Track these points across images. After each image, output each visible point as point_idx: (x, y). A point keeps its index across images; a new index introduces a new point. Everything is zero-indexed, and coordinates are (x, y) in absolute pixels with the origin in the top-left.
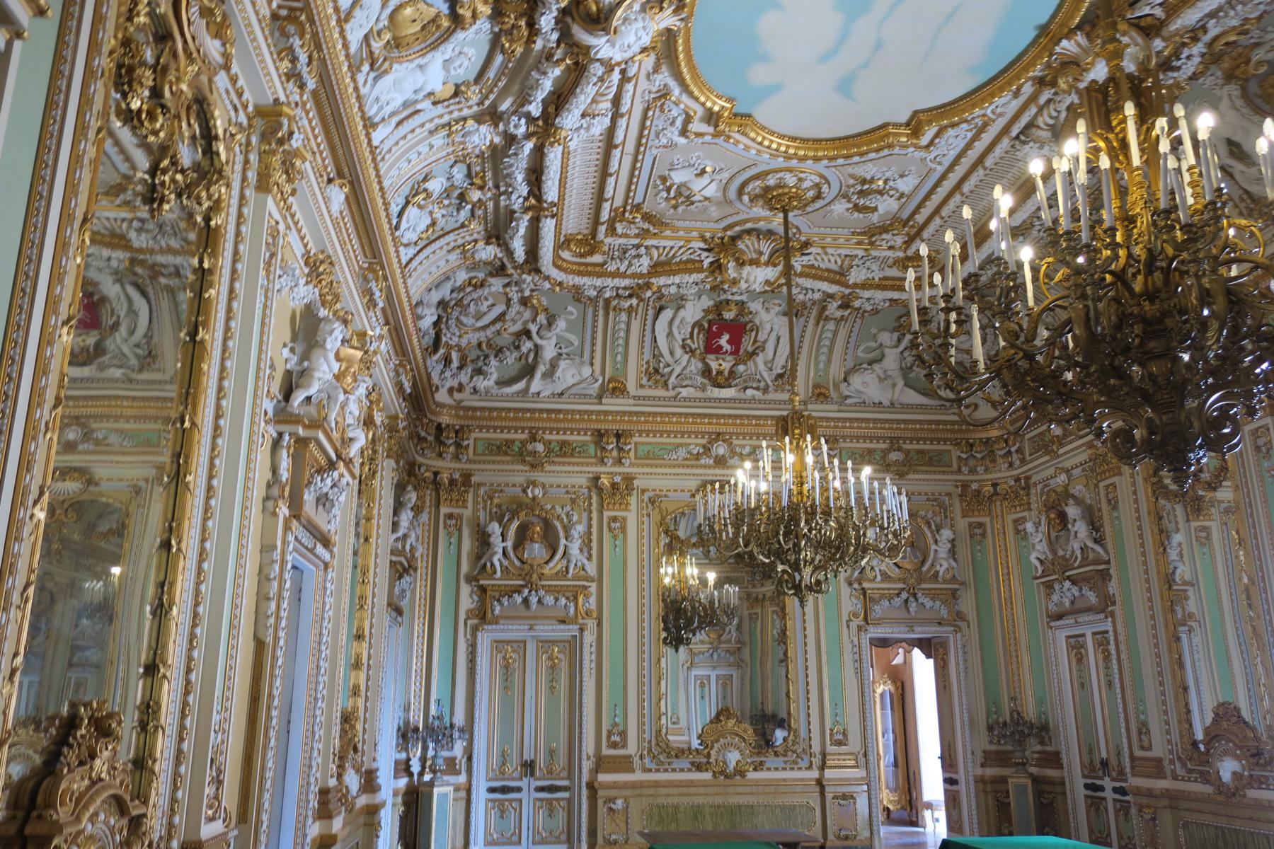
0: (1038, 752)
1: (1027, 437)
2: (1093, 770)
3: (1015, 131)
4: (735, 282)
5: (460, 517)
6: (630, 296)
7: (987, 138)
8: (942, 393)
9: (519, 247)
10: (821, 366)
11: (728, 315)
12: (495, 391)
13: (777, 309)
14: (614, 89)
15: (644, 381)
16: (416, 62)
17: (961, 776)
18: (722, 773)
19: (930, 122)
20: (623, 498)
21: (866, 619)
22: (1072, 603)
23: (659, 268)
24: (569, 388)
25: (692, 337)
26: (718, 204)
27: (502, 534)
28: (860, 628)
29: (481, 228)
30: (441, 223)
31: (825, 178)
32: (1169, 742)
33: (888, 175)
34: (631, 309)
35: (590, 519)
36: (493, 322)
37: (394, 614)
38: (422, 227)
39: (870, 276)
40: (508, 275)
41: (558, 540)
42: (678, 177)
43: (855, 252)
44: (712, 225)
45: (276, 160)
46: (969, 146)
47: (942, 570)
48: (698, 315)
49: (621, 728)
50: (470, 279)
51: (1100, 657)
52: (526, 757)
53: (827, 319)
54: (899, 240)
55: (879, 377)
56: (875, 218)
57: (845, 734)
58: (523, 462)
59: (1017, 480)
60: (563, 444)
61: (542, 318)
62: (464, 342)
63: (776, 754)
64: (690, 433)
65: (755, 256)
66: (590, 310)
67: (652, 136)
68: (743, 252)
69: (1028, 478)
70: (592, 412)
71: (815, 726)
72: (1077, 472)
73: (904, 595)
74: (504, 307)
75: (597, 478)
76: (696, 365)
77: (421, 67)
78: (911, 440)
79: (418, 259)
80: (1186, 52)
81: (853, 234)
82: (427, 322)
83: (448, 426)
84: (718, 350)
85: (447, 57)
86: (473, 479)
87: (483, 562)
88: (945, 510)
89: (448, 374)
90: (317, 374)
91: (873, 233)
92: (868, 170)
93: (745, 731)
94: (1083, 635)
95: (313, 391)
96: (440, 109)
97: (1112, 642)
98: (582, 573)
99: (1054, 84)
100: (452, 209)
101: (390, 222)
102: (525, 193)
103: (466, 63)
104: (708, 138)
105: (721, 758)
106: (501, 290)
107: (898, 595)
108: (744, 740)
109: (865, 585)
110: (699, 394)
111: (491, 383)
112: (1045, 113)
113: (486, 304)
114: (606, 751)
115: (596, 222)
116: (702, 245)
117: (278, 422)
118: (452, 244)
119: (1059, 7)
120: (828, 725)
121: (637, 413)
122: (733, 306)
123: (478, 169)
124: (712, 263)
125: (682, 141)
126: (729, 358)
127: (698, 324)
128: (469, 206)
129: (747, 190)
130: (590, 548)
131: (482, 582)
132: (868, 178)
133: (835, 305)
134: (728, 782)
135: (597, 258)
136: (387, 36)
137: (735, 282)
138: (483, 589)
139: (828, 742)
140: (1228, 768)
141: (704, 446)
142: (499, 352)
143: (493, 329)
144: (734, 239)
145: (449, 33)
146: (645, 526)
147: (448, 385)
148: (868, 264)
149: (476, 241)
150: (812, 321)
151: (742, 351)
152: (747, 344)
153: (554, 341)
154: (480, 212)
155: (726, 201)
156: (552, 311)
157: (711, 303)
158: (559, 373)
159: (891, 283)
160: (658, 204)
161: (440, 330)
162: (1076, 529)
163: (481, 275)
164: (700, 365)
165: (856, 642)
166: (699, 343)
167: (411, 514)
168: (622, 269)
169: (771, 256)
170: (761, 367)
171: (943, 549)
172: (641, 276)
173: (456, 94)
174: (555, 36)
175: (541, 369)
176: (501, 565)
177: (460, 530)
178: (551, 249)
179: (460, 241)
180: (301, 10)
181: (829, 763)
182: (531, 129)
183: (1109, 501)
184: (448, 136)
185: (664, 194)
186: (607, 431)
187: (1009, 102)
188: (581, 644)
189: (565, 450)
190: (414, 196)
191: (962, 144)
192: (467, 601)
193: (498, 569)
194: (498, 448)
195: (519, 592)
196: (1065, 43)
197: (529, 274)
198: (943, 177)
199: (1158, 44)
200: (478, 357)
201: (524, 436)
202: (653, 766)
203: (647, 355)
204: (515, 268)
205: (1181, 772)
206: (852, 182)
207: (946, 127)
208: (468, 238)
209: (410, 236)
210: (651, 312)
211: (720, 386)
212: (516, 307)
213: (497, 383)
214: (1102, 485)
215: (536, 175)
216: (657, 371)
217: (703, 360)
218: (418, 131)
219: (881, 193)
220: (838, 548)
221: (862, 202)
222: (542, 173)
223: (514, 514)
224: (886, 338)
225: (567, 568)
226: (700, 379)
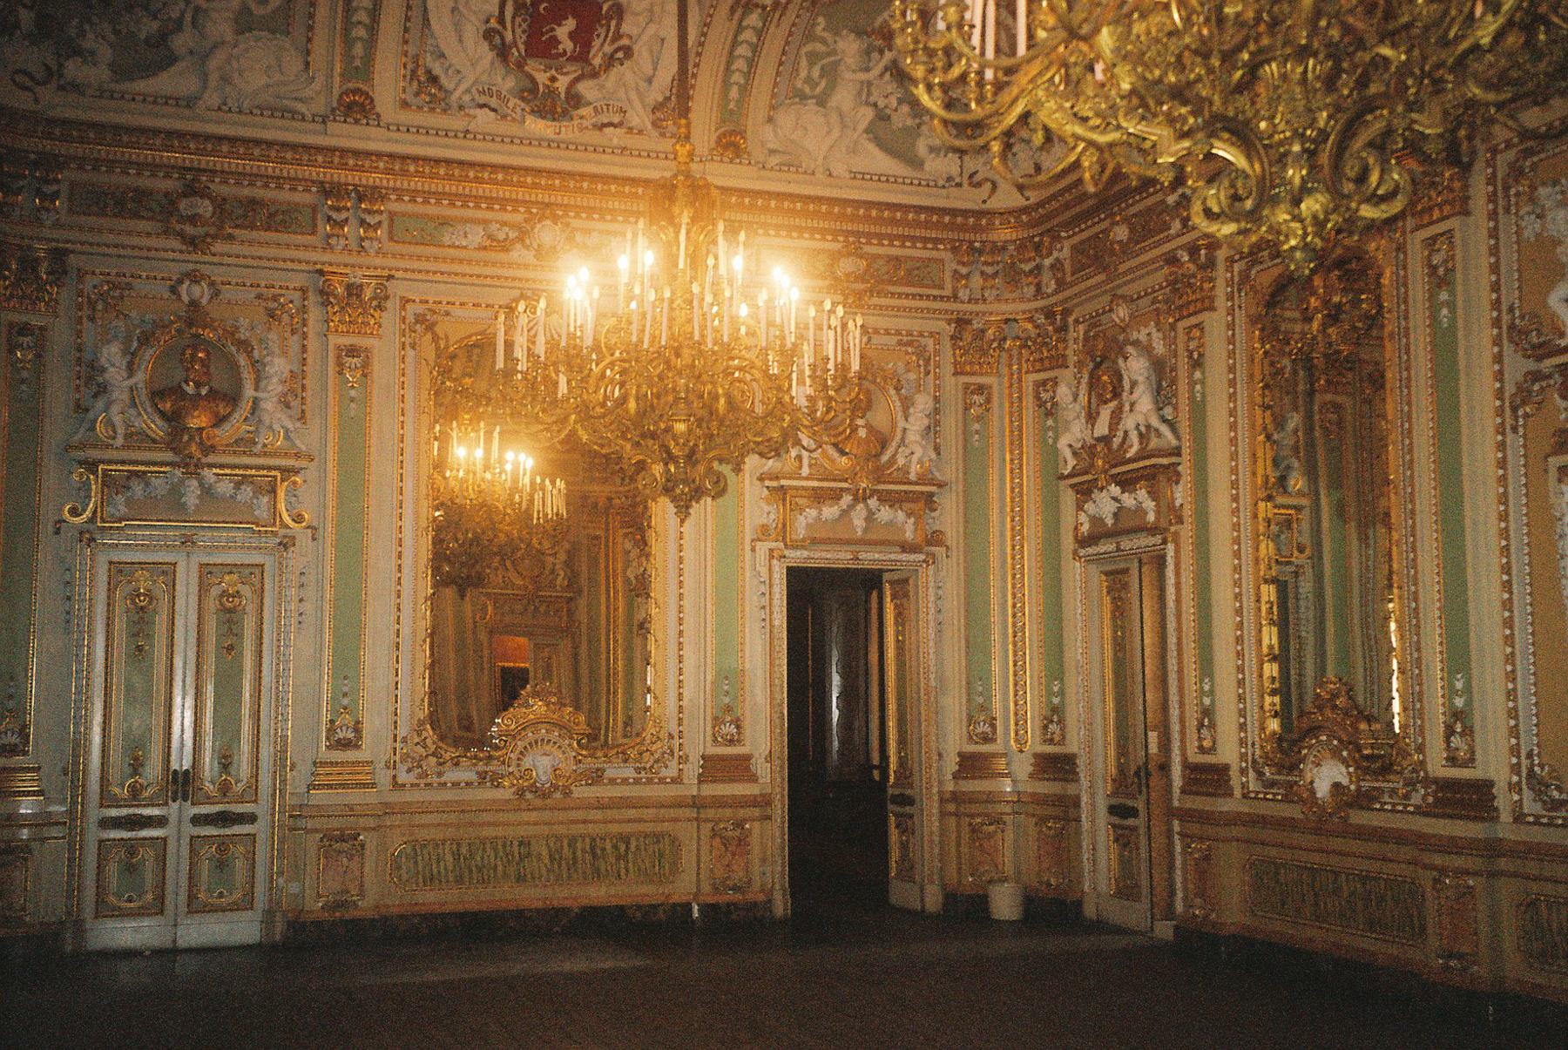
25: (501, 21)
52: (175, 766)
60: (253, 203)
88: (927, 361)
94: (1126, 571)
165: (765, 577)
211: (540, 113)
214: (1181, 325)
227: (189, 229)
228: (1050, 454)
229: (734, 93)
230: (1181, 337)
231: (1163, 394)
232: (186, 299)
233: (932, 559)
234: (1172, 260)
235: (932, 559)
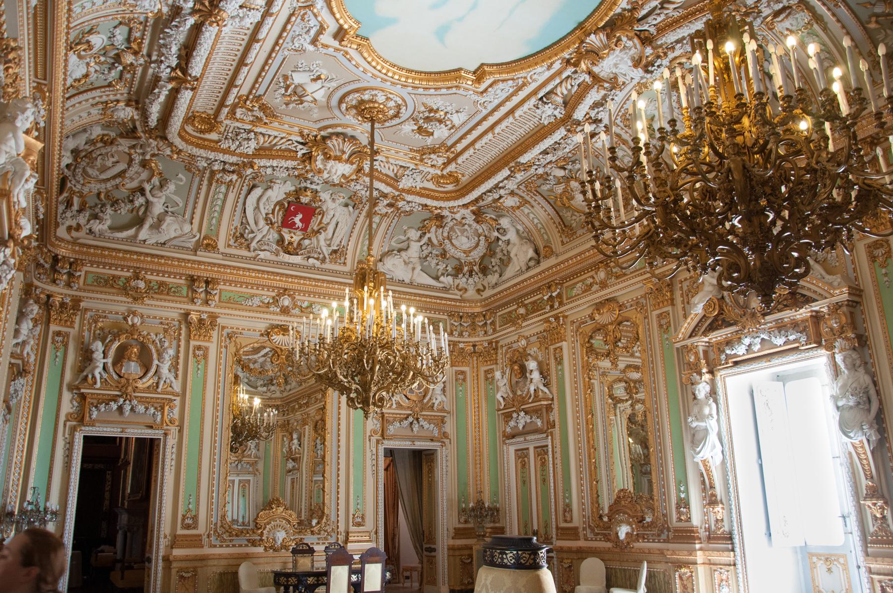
0: (491, 528)
1: (499, 314)
3: (541, 94)
4: (320, 171)
5: (67, 335)
6: (233, 172)
7: (522, 95)
9: (155, 110)
11: (304, 200)
12: (108, 234)
13: (341, 200)
15: (232, 242)
18: (271, 548)
19: (491, 73)
20: (207, 331)
21: (382, 435)
22: (524, 427)
23: (261, 152)
24: (171, 240)
25: (273, 213)
26: (321, 108)
27: (104, 352)
28: (378, 441)
29: (125, 91)
31: (404, 100)
32: (584, 516)
33: (449, 109)
35: (179, 346)
36: (114, 177)
39: (414, 185)
41: (151, 360)
42: (298, 78)
43: (408, 165)
44: (311, 125)
46: (508, 99)
47: (437, 403)
48: (282, 196)
49: (194, 513)
50: (104, 135)
51: (539, 463)
53: (376, 213)
54: (441, 161)
55: (404, 261)
56: (429, 141)
57: (363, 518)
58: (127, 295)
59: (490, 343)
60: (161, 284)
61: (156, 180)
62: (86, 190)
63: (313, 533)
64: (263, 287)
65: (338, 154)
66: (197, 180)
67: (288, 39)
68: (330, 149)
69: (497, 342)
70: (189, 261)
71: (342, 513)
73: (411, 419)
74: (126, 166)
76: (274, 236)
80: (659, 62)
81: (411, 150)
83: (64, 257)
86: (82, 304)
87: (85, 373)
89: (68, 214)
91: (424, 152)
92: (436, 102)
93: (290, 516)
94: (527, 449)
97: (550, 453)
98: (170, 389)
99: (576, 65)
100: (105, 67)
102: (174, 65)
105: (271, 536)
106: (127, 150)
107: (406, 419)
108: (289, 522)
109: (384, 410)
110: (274, 258)
111: (105, 227)
112: (564, 84)
113: (112, 160)
114: (180, 532)
115: (222, 104)
116: (300, 139)
118: (97, 99)
119: (601, 4)
120: (352, 511)
121: (225, 266)
122: (309, 193)
123: (138, 35)
124: (304, 154)
125: (311, 48)
126: (299, 233)
127: (280, 203)
128: (121, 68)
129: (347, 99)
130: (177, 370)
131: (83, 391)
132: (435, 108)
133: (386, 202)
134: (276, 554)
135: (214, 136)
137: (320, 171)
138: (83, 397)
139: (351, 524)
140: (623, 531)
141: (273, 298)
142: (115, 203)
143: (113, 182)
144: (324, 138)
146: (223, 356)
148: (415, 175)
149: (118, 101)
150: (364, 213)
151: (309, 229)
152: (314, 225)
153: (163, 200)
154: (128, 76)
155: (329, 107)
156: (166, 176)
157: (293, 188)
159: (427, 192)
160: (275, 99)
162: (532, 377)
163: (113, 134)
164: (276, 236)
165: (374, 452)
166: (278, 218)
167: (31, 325)
168: (233, 148)
169: (350, 156)
170: (322, 243)
172: (247, 156)
175: (149, 222)
177: (66, 346)
178: (181, 120)
179: (105, 98)
181: (351, 539)
183: (556, 359)
185: (283, 91)
187: (543, 72)
188: (165, 445)
189: (163, 289)
190: (77, 44)
191: (504, 95)
192: (68, 405)
195: (115, 401)
196: (593, 36)
197: (155, 139)
198: (485, 118)
199: (649, 51)
200: (96, 205)
201: (128, 274)
202: (218, 543)
203: (237, 223)
204: (145, 132)
206: (422, 109)
207: (498, 81)
208: (112, 97)
210: (245, 189)
211: (289, 253)
212: (136, 168)
213: (110, 228)
216: (242, 235)
217: (279, 232)
219: (440, 121)
220: (399, 374)
221: (426, 126)
222: (193, 49)
223: (116, 336)
224: (414, 234)
225: (158, 384)
226: (275, 246)
231: (544, 374)
232: (130, 323)
233: (443, 444)
235: (443, 444)
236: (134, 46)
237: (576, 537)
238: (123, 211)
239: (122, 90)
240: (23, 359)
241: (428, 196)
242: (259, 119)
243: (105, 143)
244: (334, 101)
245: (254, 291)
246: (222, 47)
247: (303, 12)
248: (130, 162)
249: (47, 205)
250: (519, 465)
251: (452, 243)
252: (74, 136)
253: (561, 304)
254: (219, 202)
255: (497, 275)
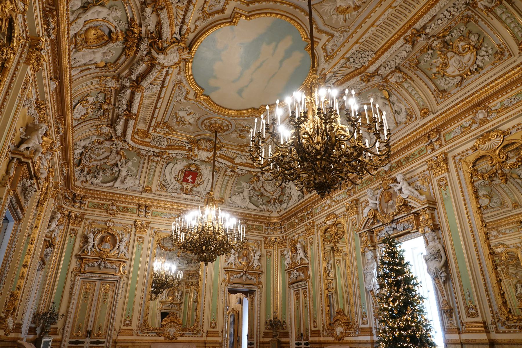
2: (298, 338)
6: (158, 156)
8: (261, 206)
9: (119, 131)
10: (222, 192)
11: (193, 169)
14: (163, 77)
15: (159, 189)
16: (93, 50)
17: (255, 342)
18: (168, 337)
20: (144, 230)
23: (169, 147)
27: (94, 239)
30: (90, 114)
31: (229, 122)
34: (157, 162)
35: (130, 236)
36: (104, 159)
37: (42, 263)
38: (82, 114)
40: (112, 141)
42: (181, 114)
45: (34, 55)
47: (255, 266)
51: (304, 297)
52: (88, 329)
53: (226, 175)
59: (283, 237)
60: (125, 207)
62: (91, 165)
66: (143, 160)
67: (174, 97)
72: (301, 234)
73: (242, 274)
74: (109, 154)
75: (135, 222)
77: (93, 52)
78: (250, 220)
79: (78, 127)
82: (79, 151)
83: (78, 195)
84: (187, 181)
85: (104, 51)
89: (82, 175)
90: (33, 141)
95: (30, 145)
96: (98, 70)
101: (71, 108)
102: (125, 109)
103: (111, 55)
104: (193, 101)
106: (109, 147)
111: (99, 181)
114: (123, 327)
116: (187, 141)
117: (12, 153)
121: (154, 199)
124: (189, 148)
125: (185, 101)
126: (191, 184)
127: (181, 171)
128: (102, 110)
135: (148, 140)
136: (83, 37)
138: (82, 259)
143: (103, 161)
145: (107, 43)
147: (81, 179)
149: (103, 125)
150: (221, 175)
152: (198, 180)
153: (127, 169)
154: (107, 114)
157: (187, 164)
158: (126, 181)
161: (82, 158)
163: (102, 139)
166: (181, 177)
168: (157, 145)
170: (202, 189)
171: (257, 258)
172: (164, 149)
173: (105, 66)
174: (145, 52)
176: (91, 250)
179: (96, 124)
180: (55, 10)
182: (131, 85)
184: (99, 81)
186: (142, 204)
189: (125, 210)
193: (90, 252)
194: (98, 206)
200: (96, 171)
205: (325, 334)
208: (100, 123)
209: (77, 116)
210: (165, 164)
211: (186, 194)
212: (114, 154)
214: (308, 238)
215: (130, 103)
218: (88, 76)
225: (118, 254)
226: (179, 191)
227: (111, 212)
228: (283, 265)
229: (222, 192)
230: (308, 240)
234: (306, 225)
236: (107, 101)
237: (319, 336)
238: (108, 174)
239: (104, 120)
240: (51, 238)
241: (249, 167)
242: (167, 132)
243: (99, 143)
244: (199, 124)
245: (169, 211)
246: (146, 102)
247: (178, 86)
248: (111, 152)
249: (68, 170)
250: (295, 299)
251: (265, 190)
252: (84, 140)
253: (312, 216)
254: (153, 170)
255: (286, 204)
